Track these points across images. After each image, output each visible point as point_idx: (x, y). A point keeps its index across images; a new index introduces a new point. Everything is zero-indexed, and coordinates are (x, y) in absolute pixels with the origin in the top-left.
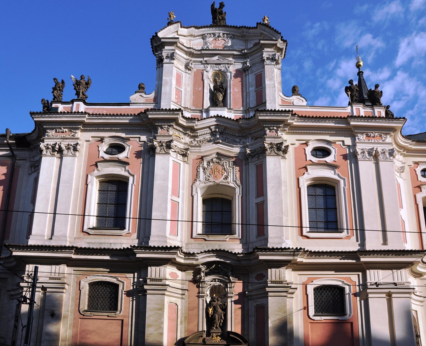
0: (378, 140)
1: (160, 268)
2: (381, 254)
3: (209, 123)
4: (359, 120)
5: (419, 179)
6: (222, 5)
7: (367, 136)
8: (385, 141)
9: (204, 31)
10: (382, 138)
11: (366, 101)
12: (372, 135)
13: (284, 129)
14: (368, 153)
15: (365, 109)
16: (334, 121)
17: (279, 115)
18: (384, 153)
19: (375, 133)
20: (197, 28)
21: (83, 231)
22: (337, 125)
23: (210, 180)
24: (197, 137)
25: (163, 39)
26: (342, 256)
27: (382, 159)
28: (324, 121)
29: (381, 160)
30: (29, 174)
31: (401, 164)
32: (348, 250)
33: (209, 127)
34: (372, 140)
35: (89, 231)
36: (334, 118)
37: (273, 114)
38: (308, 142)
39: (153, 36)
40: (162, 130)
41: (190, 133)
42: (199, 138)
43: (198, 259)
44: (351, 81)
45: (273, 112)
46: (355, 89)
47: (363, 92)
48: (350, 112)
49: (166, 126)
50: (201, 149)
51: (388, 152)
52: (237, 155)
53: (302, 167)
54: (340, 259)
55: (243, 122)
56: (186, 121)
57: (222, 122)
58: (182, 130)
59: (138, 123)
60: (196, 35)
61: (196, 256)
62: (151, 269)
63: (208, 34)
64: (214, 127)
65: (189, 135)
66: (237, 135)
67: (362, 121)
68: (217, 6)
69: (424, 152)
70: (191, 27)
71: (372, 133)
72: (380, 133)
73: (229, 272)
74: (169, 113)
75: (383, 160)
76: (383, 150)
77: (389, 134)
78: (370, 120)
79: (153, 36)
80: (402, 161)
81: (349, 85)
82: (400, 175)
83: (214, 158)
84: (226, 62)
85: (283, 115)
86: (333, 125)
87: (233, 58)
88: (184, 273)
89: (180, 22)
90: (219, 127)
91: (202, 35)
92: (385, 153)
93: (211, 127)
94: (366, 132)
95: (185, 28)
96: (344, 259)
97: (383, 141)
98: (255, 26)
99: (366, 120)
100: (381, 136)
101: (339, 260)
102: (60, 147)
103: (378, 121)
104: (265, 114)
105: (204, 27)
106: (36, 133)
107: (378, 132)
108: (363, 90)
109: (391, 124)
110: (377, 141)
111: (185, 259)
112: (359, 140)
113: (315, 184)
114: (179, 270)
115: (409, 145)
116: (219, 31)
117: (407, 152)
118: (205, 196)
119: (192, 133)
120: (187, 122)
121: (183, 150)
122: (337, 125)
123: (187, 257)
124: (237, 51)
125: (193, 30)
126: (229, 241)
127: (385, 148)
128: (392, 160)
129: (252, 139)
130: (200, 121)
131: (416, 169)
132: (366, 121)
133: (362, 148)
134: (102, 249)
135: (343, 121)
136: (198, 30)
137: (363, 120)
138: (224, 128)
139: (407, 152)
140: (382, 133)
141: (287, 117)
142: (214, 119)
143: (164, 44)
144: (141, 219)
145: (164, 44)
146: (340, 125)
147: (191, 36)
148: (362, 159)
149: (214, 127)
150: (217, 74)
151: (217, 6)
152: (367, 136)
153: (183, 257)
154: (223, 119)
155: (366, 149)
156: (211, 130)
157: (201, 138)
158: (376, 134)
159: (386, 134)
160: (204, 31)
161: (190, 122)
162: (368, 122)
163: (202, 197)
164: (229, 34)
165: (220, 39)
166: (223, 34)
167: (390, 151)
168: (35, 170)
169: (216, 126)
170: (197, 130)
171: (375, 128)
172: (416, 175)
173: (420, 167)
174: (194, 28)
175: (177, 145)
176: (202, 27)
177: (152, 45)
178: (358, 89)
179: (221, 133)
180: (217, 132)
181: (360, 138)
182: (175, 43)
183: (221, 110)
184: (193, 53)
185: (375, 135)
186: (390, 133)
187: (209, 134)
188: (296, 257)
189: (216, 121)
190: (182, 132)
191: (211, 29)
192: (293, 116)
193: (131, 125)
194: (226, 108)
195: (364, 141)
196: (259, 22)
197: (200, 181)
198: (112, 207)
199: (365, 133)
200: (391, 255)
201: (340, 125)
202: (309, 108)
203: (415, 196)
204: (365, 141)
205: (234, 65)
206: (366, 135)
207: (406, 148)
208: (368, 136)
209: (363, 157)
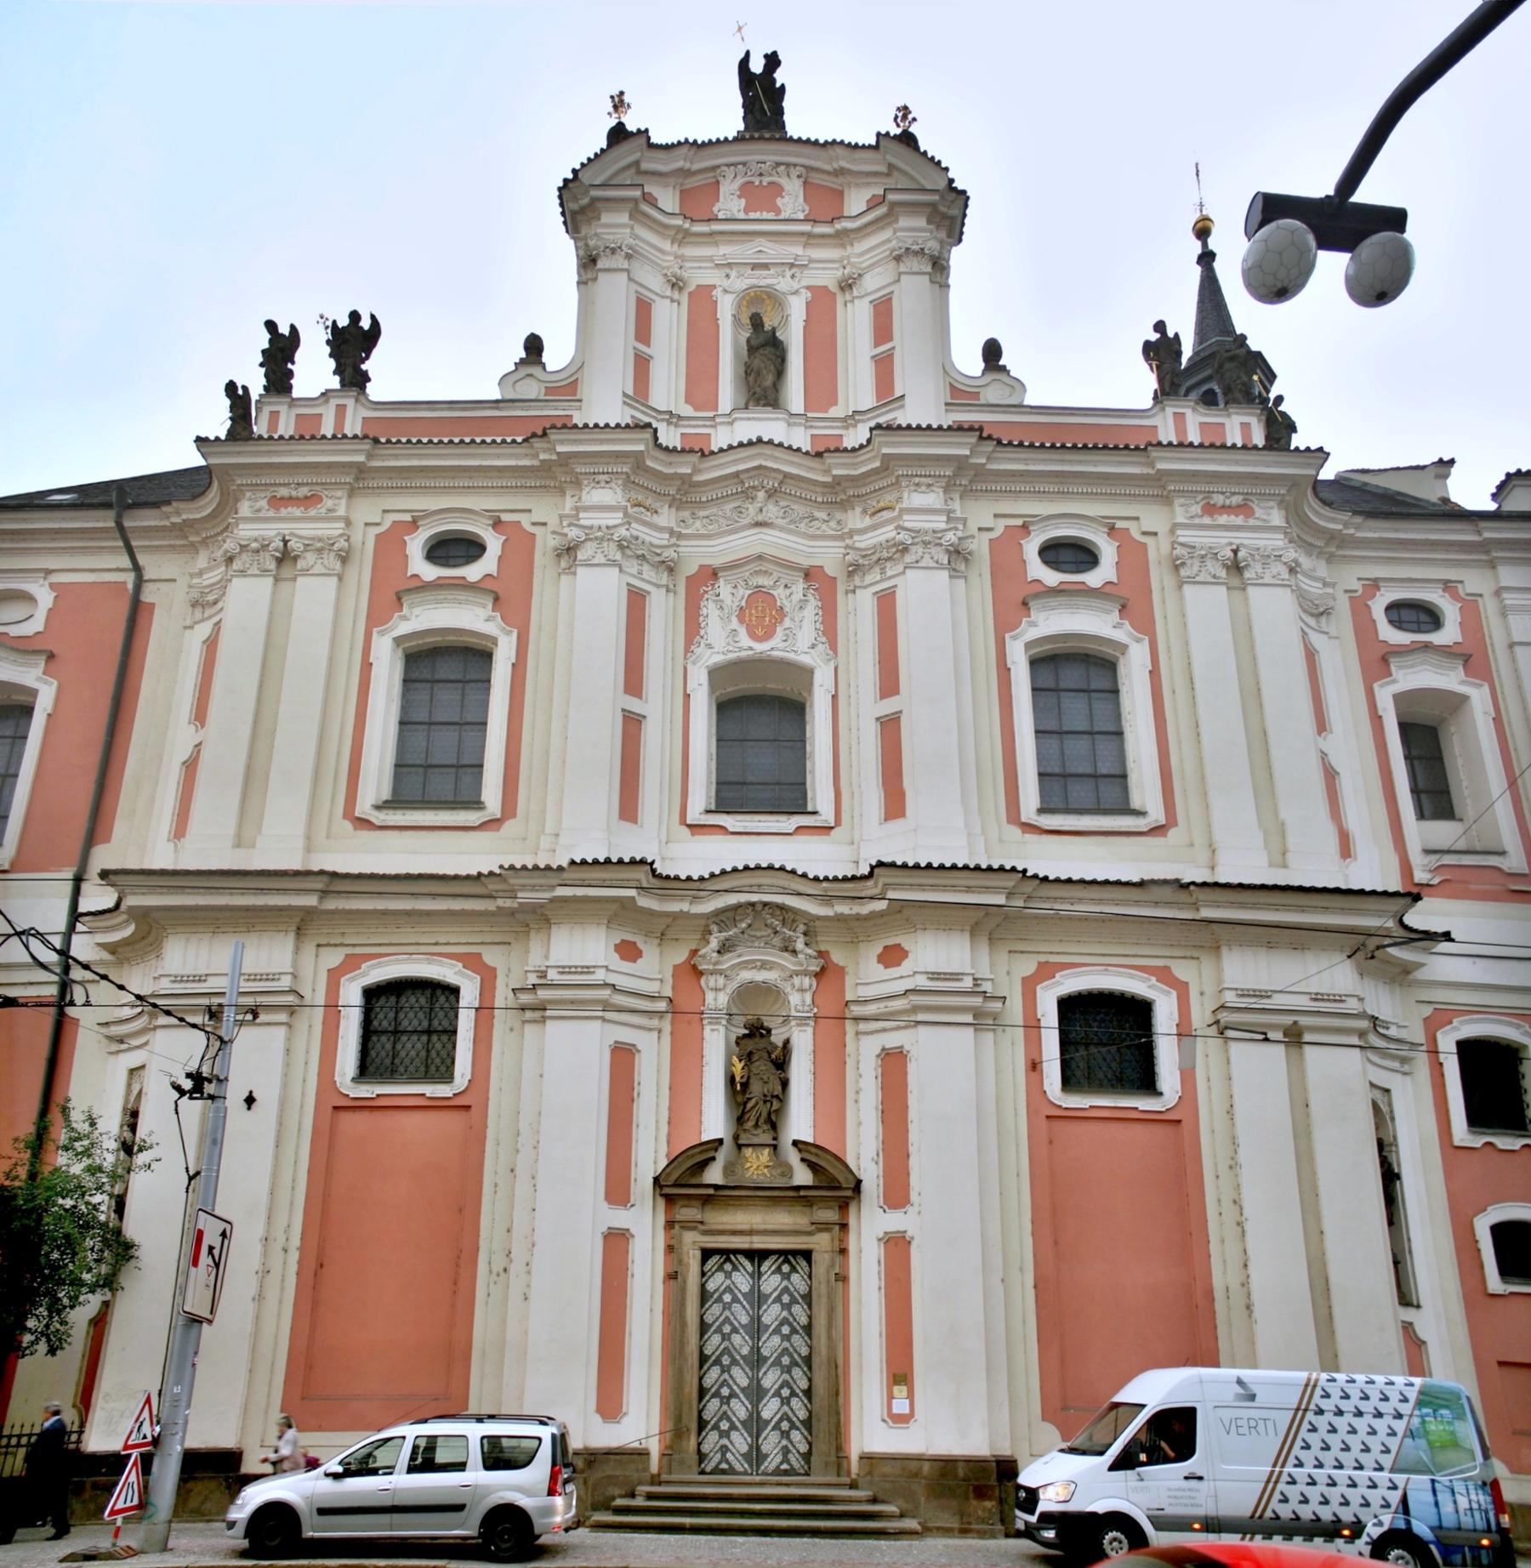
6: (773, 61)
23: (1234, 993)
30: (186, 628)
31: (1320, 585)
35: (380, 818)
63: (728, 165)
68: (757, 66)
81: (1154, 337)
98: (873, 142)
106: (212, 495)
129: (864, 512)
138: (781, 477)
144: (452, 766)
151: (757, 66)
168: (206, 615)
175: (640, 534)
177: (562, 205)
178: (1187, 351)
196: (883, 132)
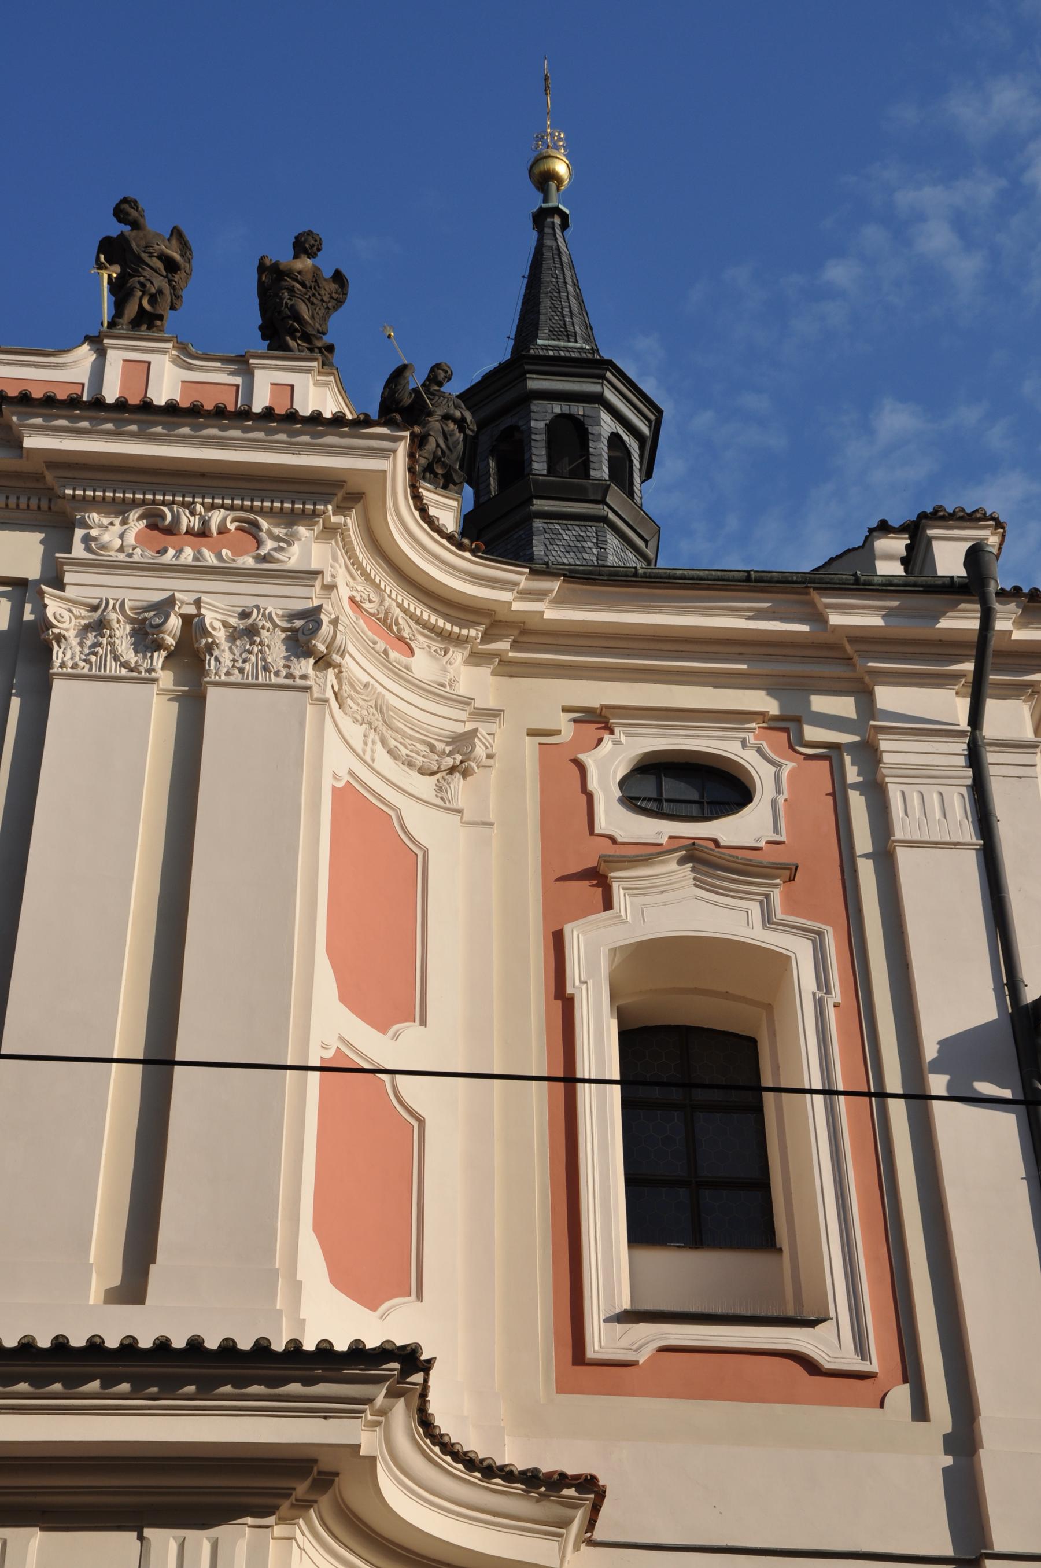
0: (224, 552)
4: (85, 424)
5: (602, 824)
7: (155, 523)
8: (278, 561)
10: (259, 543)
11: (527, 367)
12: (186, 520)
14: (134, 633)
15: (190, 368)
18: (251, 632)
19: (213, 507)
27: (228, 674)
29: (223, 678)
34: (180, 552)
44: (126, 206)
46: (151, 255)
47: (542, 317)
48: (86, 381)
51: (284, 630)
69: (624, 644)
71: (183, 504)
72: (242, 508)
75: (236, 677)
76: (245, 615)
77: (308, 518)
78: (159, 429)
80: (465, 702)
81: (115, 229)
82: (440, 789)
92: (258, 634)
94: (144, 502)
97: (265, 559)
99: (134, 428)
100: (251, 529)
102: (193, 625)
103: (213, 431)
107: (228, 502)
108: (542, 310)
109: (309, 453)
110: (219, 557)
112: (88, 549)
115: (515, 599)
117: (515, 645)
127: (261, 602)
128: (299, 682)
131: (589, 759)
132: (132, 435)
133: (93, 595)
137: (109, 426)
139: (515, 645)
140: (261, 511)
148: (86, 671)
152: (152, 526)
155: (122, 604)
158: (216, 517)
159: (291, 519)
162: (143, 436)
167: (298, 623)
171: (203, 475)
172: (584, 798)
173: (617, 742)
181: (95, 539)
185: (205, 522)
186: (314, 514)
195: (122, 557)
199: (134, 504)
200: (95, 1385)
203: (558, 942)
204: (130, 555)
206: (143, 523)
207: (500, 617)
208: (160, 525)
209: (93, 658)
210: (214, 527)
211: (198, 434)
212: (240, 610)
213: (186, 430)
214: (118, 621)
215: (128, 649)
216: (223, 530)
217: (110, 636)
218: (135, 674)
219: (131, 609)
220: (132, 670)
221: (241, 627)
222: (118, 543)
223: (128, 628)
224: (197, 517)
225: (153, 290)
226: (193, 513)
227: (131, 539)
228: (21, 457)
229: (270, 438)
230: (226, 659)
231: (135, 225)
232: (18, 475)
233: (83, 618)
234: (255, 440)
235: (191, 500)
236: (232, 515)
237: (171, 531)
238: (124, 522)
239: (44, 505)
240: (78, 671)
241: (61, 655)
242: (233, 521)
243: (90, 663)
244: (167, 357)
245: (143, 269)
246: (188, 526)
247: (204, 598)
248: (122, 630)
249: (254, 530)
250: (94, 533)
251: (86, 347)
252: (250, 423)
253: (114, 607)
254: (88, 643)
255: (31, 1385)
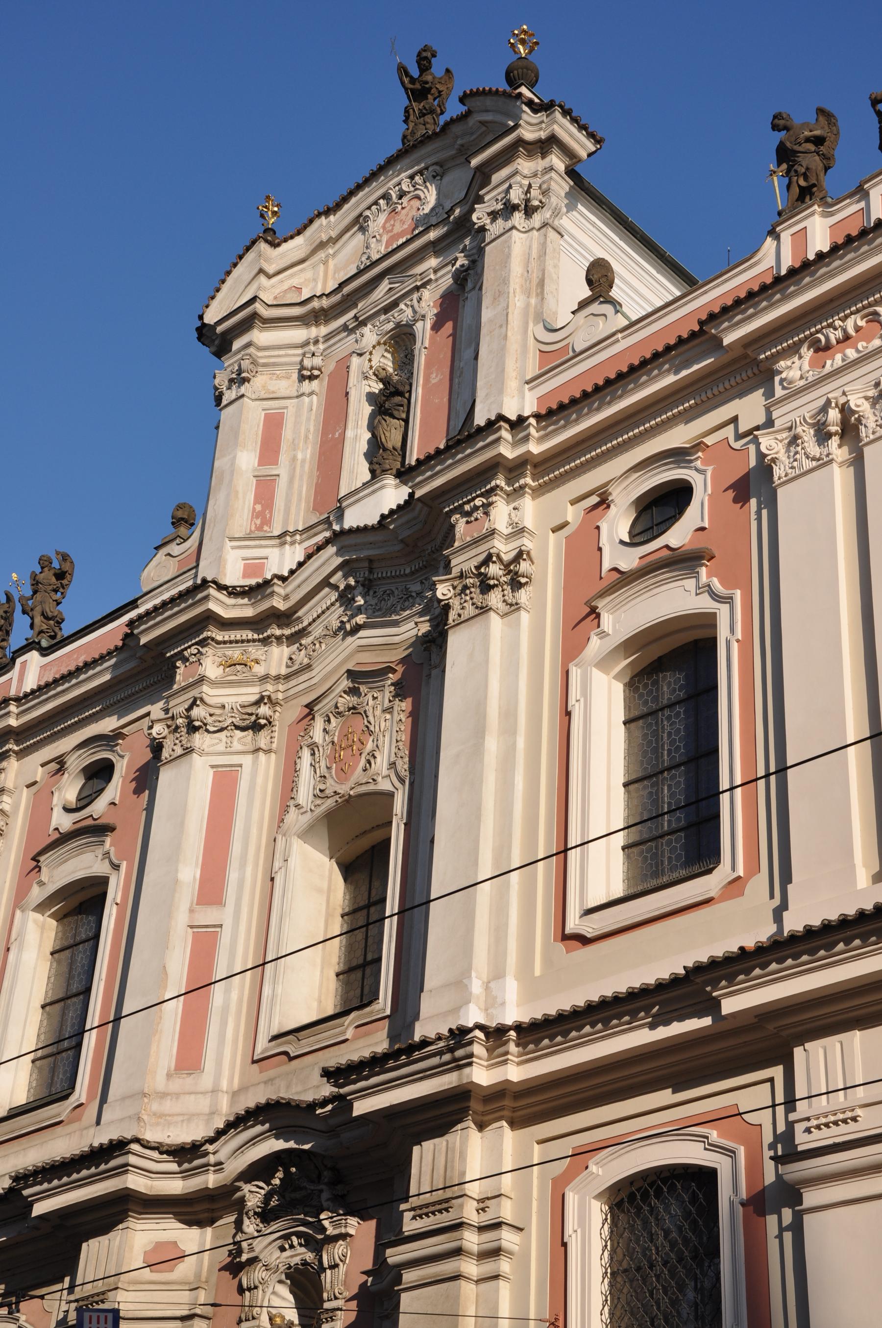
1: (435, 1145)
2: (812, 952)
3: (322, 569)
4: (751, 311)
7: (822, 349)
9: (358, 204)
12: (834, 336)
13: (517, 485)
15: (831, 214)
16: (667, 366)
17: (469, 451)
20: (328, 212)
21: (566, 938)
22: (684, 373)
24: (302, 633)
25: (220, 324)
26: (647, 1009)
27: (874, 433)
28: (632, 386)
32: (622, 988)
33: (325, 583)
35: (591, 927)
36: (656, 356)
37: (450, 461)
38: (605, 492)
39: (198, 329)
40: (186, 666)
41: (278, 632)
42: (310, 632)
43: (221, 1163)
45: (447, 455)
49: (193, 648)
50: (313, 673)
52: (411, 650)
53: (584, 615)
54: (653, 1026)
55: (400, 522)
56: (249, 600)
57: (355, 547)
58: (249, 634)
59: (133, 669)
60: (333, 234)
61: (206, 1154)
62: (422, 1152)
64: (340, 574)
65: (279, 639)
66: (408, 571)
67: (765, 308)
70: (311, 221)
72: (864, 308)
73: (321, 1191)
74: (183, 605)
78: (792, 288)
79: (198, 329)
83: (341, 696)
84: (409, 285)
85: (481, 444)
86: (670, 379)
87: (437, 254)
88: (209, 1230)
89: (260, 237)
90: (355, 565)
91: (356, 220)
93: (333, 580)
94: (806, 338)
95: (292, 237)
96: (667, 1023)
99: (778, 296)
101: (646, 1030)
102: (845, 410)
104: (429, 473)
105: (352, 193)
107: (854, 308)
111: (186, 1174)
112: (784, 388)
113: (660, 658)
114: (190, 1223)
116: (397, 176)
118: (342, 851)
119: (288, 625)
120: (253, 601)
121: (249, 710)
122: (684, 373)
123: (186, 1166)
124: (437, 224)
125: (321, 225)
126: (356, 1038)
130: (289, 580)
132: (779, 301)
134: (850, 921)
135: (694, 347)
136: (339, 213)
138: (366, 564)
141: (495, 445)
142: (331, 550)
143: (228, 337)
145: (228, 337)
146: (696, 367)
147: (322, 245)
148: (793, 474)
149: (340, 574)
150: (396, 342)
152: (817, 351)
153: (174, 1167)
154: (352, 536)
156: (335, 587)
157: (317, 631)
160: (358, 204)
161: (259, 597)
162: (786, 298)
163: (333, 860)
164: (427, 168)
165: (405, 200)
166: (412, 177)
169: (346, 569)
170: (296, 612)
174: (323, 217)
176: (345, 200)
179: (367, 586)
180: (354, 588)
182: (255, 318)
183: (374, 492)
184: (322, 309)
187: (338, 604)
188: (467, 1070)
189: (338, 554)
190: (254, 641)
191: (375, 184)
192: (519, 429)
193: (120, 682)
194: (386, 479)
197: (297, 806)
198: (680, 776)
199: (801, 342)
200: (841, 946)
201: (696, 367)
202: (623, 338)
205: (436, 280)
209: (795, 464)
210: (851, 331)
211: (815, 277)
212: (873, 383)
213: (807, 279)
214: (804, 431)
215: (814, 446)
216: (858, 329)
217: (802, 443)
218: (821, 462)
219: (811, 418)
220: (819, 460)
221: (876, 394)
222: (798, 373)
223: (812, 432)
224: (839, 329)
225: (803, 170)
226: (835, 329)
227: (806, 367)
228: (728, 351)
229: (872, 246)
230: (871, 424)
231: (787, 128)
232: (734, 361)
233: (786, 438)
234: (850, 261)
235: (831, 320)
236: (858, 316)
237: (828, 347)
238: (800, 357)
239: (756, 371)
240: (790, 476)
241: (778, 470)
242: (862, 319)
243: (795, 468)
244: (817, 217)
245: (798, 157)
246: (836, 338)
247: (846, 389)
248: (808, 435)
249: (876, 318)
250: (784, 375)
251: (769, 239)
252: (842, 252)
253: (800, 423)
254: (792, 454)
255: (808, 955)
